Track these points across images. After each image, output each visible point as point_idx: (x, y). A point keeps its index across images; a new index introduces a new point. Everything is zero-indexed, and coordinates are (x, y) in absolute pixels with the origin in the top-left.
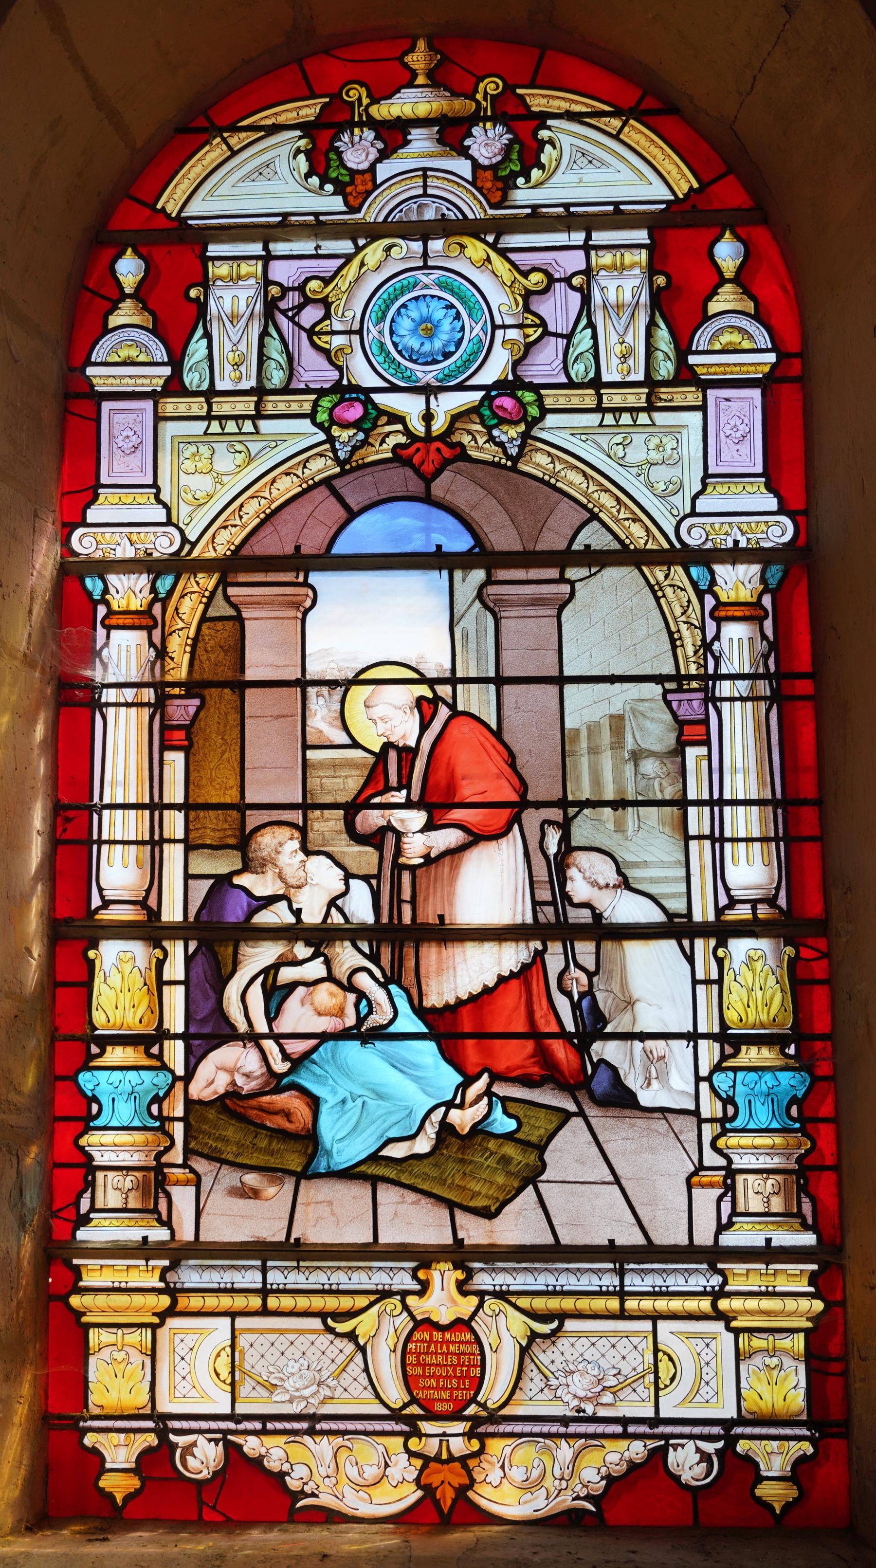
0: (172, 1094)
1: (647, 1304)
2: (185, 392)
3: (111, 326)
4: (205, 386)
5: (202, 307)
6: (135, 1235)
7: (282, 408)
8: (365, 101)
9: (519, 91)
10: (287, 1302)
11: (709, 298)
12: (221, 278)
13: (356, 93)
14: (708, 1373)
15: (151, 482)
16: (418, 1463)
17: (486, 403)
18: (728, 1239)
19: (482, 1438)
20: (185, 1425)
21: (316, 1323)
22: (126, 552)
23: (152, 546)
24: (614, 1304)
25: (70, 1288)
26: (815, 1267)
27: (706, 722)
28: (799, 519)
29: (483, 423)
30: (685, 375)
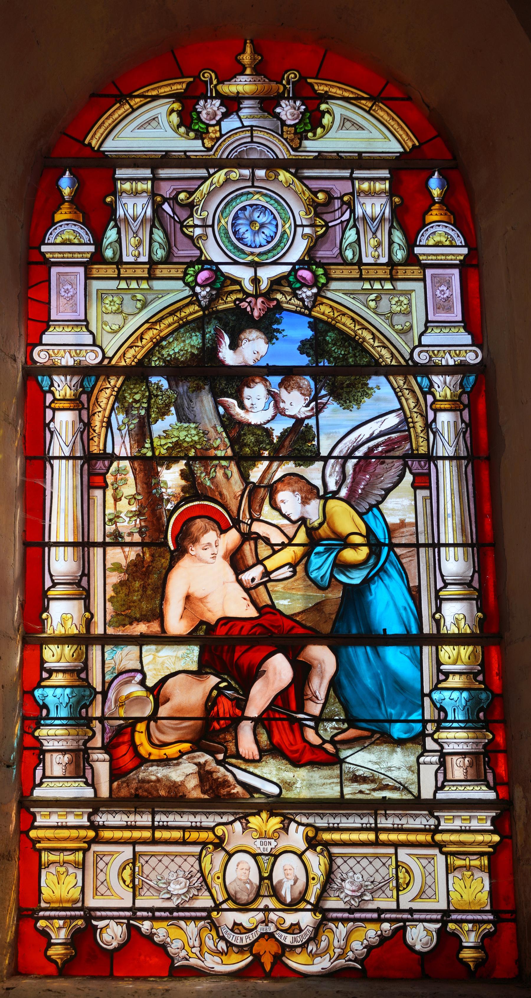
0: (94, 702)
1: (393, 837)
3: (56, 220)
4: (116, 259)
5: (112, 209)
7: (165, 273)
8: (215, 82)
9: (309, 81)
10: (166, 834)
12: (125, 192)
13: (208, 75)
14: (429, 880)
15: (83, 318)
17: (293, 273)
18: (441, 795)
20: (104, 913)
22: (68, 361)
23: (84, 359)
24: (372, 836)
25: (29, 826)
27: (429, 474)
29: (290, 285)
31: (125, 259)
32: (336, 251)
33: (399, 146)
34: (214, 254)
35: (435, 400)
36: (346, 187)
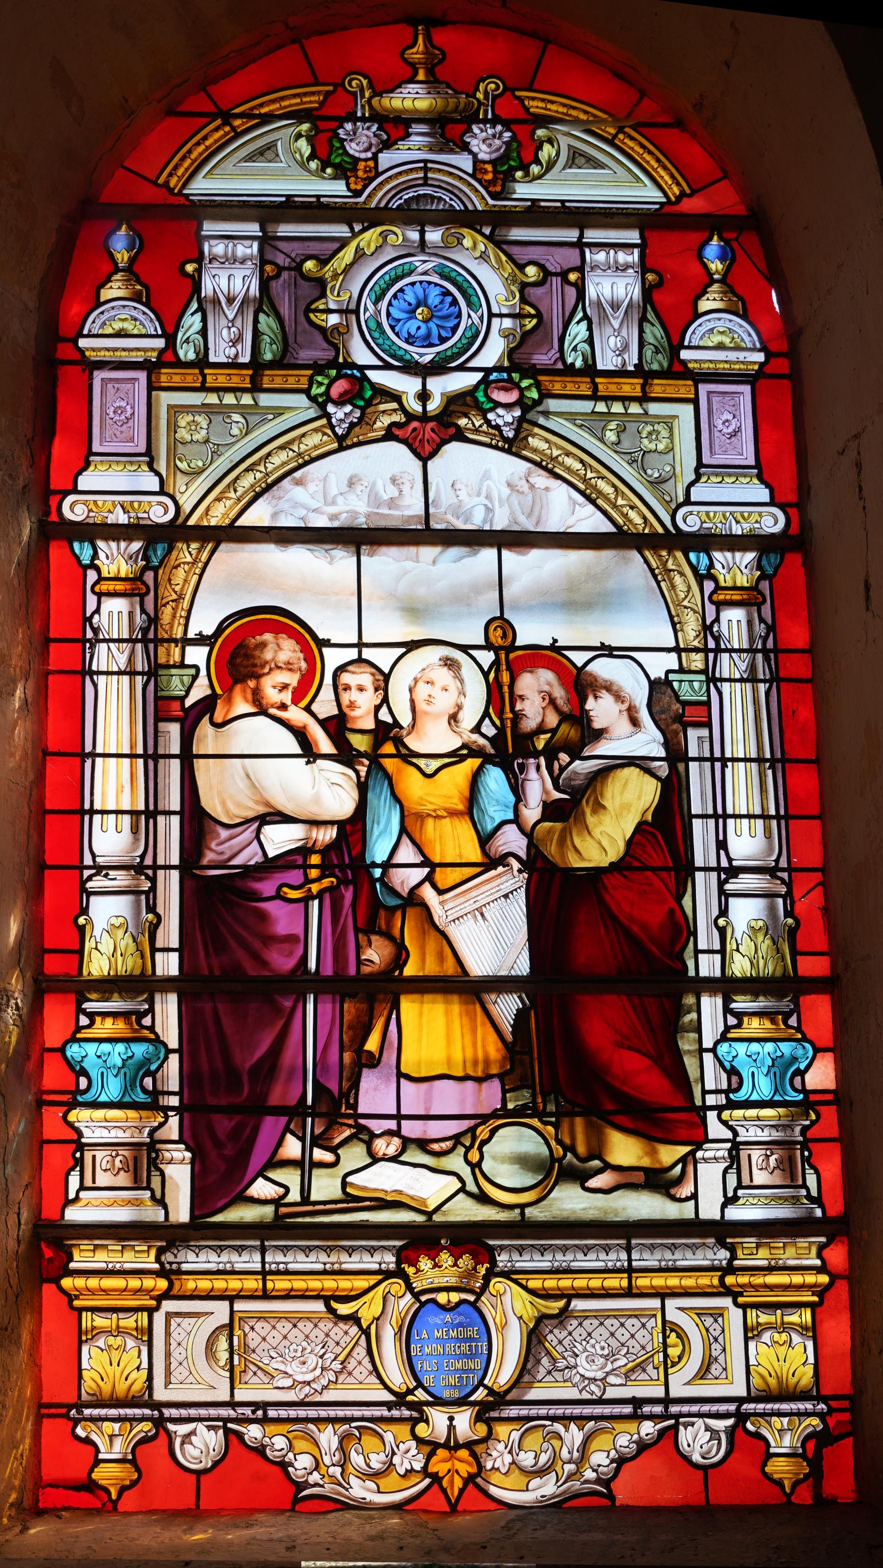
1: (658, 1281)
2: (179, 364)
3: (102, 300)
6: (122, 1215)
7: (278, 383)
8: (367, 94)
9: (518, 93)
11: (102, 285)
16: (427, 1449)
18: (734, 1213)
19: (489, 1423)
21: (319, 1306)
26: (823, 1239)
27: (708, 704)
28: (791, 511)
30: (678, 370)
31: (212, 359)
32: (554, 353)
33: (660, 194)
34: (361, 355)
35: (718, 588)
36: (571, 257)
